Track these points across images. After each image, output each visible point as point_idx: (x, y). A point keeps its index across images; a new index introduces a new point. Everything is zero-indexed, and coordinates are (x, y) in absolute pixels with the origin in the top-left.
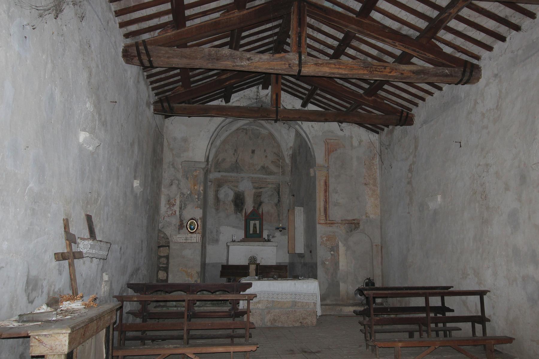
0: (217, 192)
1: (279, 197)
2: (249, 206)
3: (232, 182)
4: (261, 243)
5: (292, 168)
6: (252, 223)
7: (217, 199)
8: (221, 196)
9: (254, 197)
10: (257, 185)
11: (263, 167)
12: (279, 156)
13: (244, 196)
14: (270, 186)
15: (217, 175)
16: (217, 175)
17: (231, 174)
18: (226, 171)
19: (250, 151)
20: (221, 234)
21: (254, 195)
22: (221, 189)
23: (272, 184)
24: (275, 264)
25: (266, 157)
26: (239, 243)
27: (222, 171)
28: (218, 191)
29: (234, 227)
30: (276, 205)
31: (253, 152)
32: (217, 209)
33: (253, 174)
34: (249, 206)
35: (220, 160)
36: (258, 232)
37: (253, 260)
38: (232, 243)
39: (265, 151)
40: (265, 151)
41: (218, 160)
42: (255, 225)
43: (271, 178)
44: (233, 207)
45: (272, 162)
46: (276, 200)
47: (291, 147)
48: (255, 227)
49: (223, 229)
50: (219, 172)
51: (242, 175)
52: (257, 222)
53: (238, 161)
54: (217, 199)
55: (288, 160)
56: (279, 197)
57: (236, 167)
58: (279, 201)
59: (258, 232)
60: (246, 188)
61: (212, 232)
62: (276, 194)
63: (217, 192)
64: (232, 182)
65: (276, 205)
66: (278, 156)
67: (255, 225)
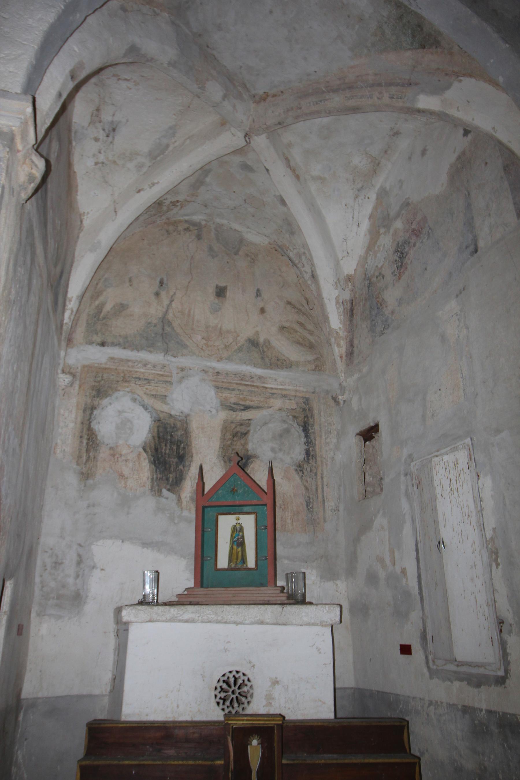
0: (89, 410)
1: (309, 442)
2: (208, 460)
3: (148, 381)
4: (269, 612)
5: (351, 344)
6: (226, 523)
7: (89, 439)
8: (106, 425)
9: (223, 439)
10: (233, 398)
11: (253, 343)
12: (305, 310)
13: (187, 432)
14: (278, 403)
15: (97, 355)
16: (97, 355)
17: (143, 355)
18: (126, 343)
19: (211, 290)
20: (97, 573)
21: (225, 429)
23: (285, 396)
24: (325, 711)
25: (263, 311)
26: (173, 611)
27: (113, 344)
28: (93, 408)
29: (145, 544)
30: (300, 468)
31: (221, 292)
32: (86, 476)
33: (220, 360)
34: (208, 460)
35: (108, 307)
36: (251, 563)
37: (233, 689)
38: (144, 612)
39: (258, 293)
40: (258, 293)
41: (100, 308)
42: (237, 532)
43: (277, 379)
44: (145, 470)
45: (282, 328)
46: (298, 452)
47: (349, 278)
48: (238, 540)
49: (103, 551)
50: (103, 344)
51: (183, 361)
52: (248, 522)
53: (170, 316)
54: (89, 439)
55: (336, 321)
56: (309, 442)
57: (162, 335)
58: (309, 455)
59: (251, 563)
60: (196, 401)
61: (57, 564)
62: (297, 431)
63: (89, 410)
64: (148, 381)
65: (300, 468)
66: (299, 311)
67: (237, 532)
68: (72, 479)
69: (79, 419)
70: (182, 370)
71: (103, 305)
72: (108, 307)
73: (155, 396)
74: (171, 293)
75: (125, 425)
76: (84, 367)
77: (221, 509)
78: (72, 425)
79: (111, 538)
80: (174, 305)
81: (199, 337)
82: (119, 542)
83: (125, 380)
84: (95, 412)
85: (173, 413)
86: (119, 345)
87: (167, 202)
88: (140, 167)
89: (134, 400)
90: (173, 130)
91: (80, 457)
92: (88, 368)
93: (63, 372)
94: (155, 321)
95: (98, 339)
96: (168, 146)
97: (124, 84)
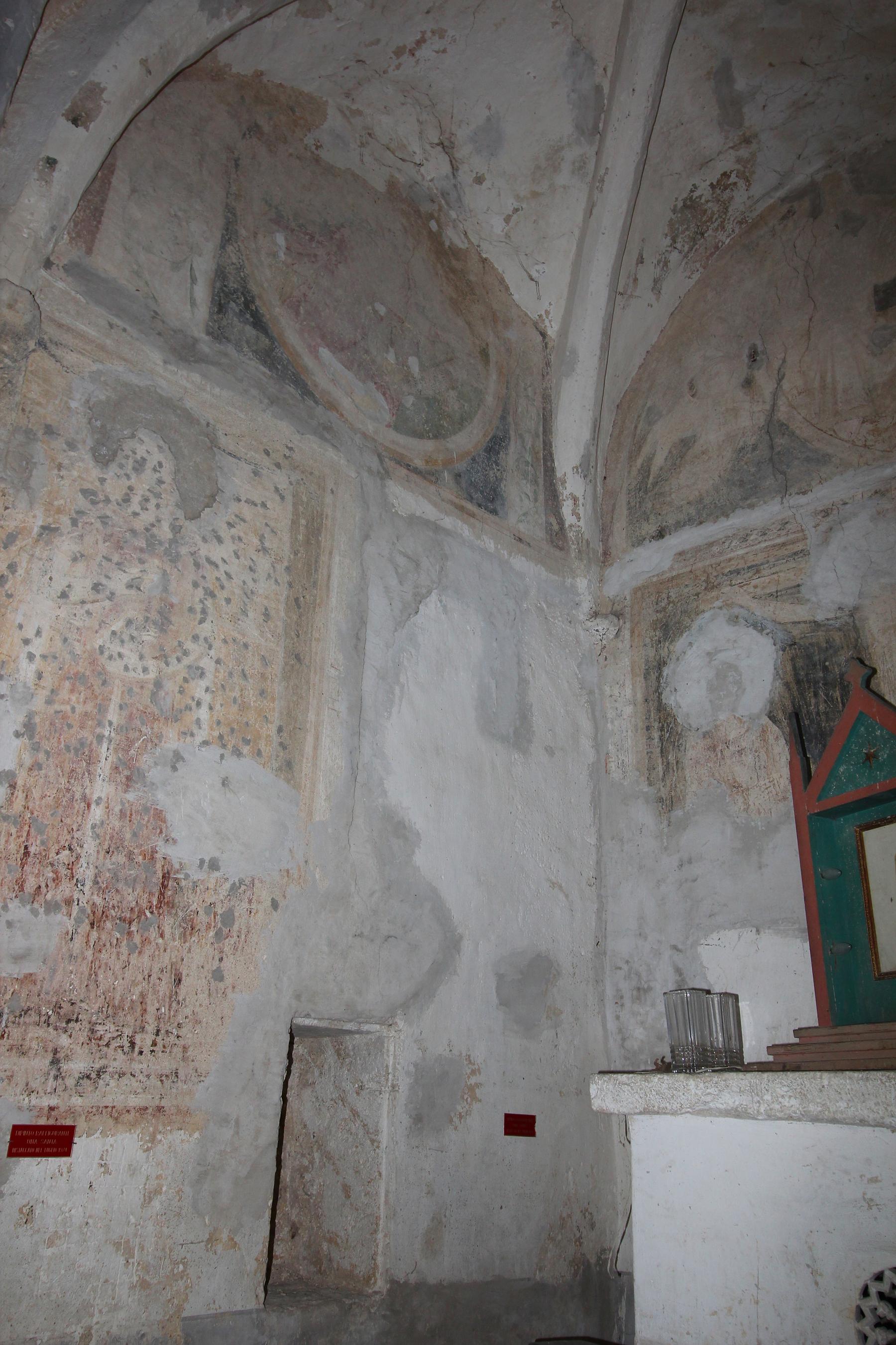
0: (655, 672)
8: (689, 696)
15: (651, 560)
16: (651, 560)
17: (738, 520)
22: (680, 644)
27: (679, 525)
28: (661, 664)
32: (667, 803)
35: (659, 461)
41: (645, 471)
50: (661, 534)
54: (663, 726)
63: (655, 672)
64: (756, 569)
68: (643, 814)
69: (640, 697)
70: (826, 513)
71: (650, 459)
72: (659, 461)
73: (775, 596)
74: (776, 364)
75: (724, 679)
76: (636, 591)
77: (872, 813)
78: (628, 710)
79: (733, 925)
80: (786, 385)
81: (854, 423)
82: (749, 935)
83: (711, 586)
84: (666, 671)
85: (820, 617)
86: (691, 521)
87: (704, 190)
88: (579, 168)
89: (734, 620)
90: (579, 48)
91: (651, 768)
92: (640, 592)
93: (595, 615)
94: (751, 441)
95: (651, 528)
96: (598, 89)
97: (425, 52)
